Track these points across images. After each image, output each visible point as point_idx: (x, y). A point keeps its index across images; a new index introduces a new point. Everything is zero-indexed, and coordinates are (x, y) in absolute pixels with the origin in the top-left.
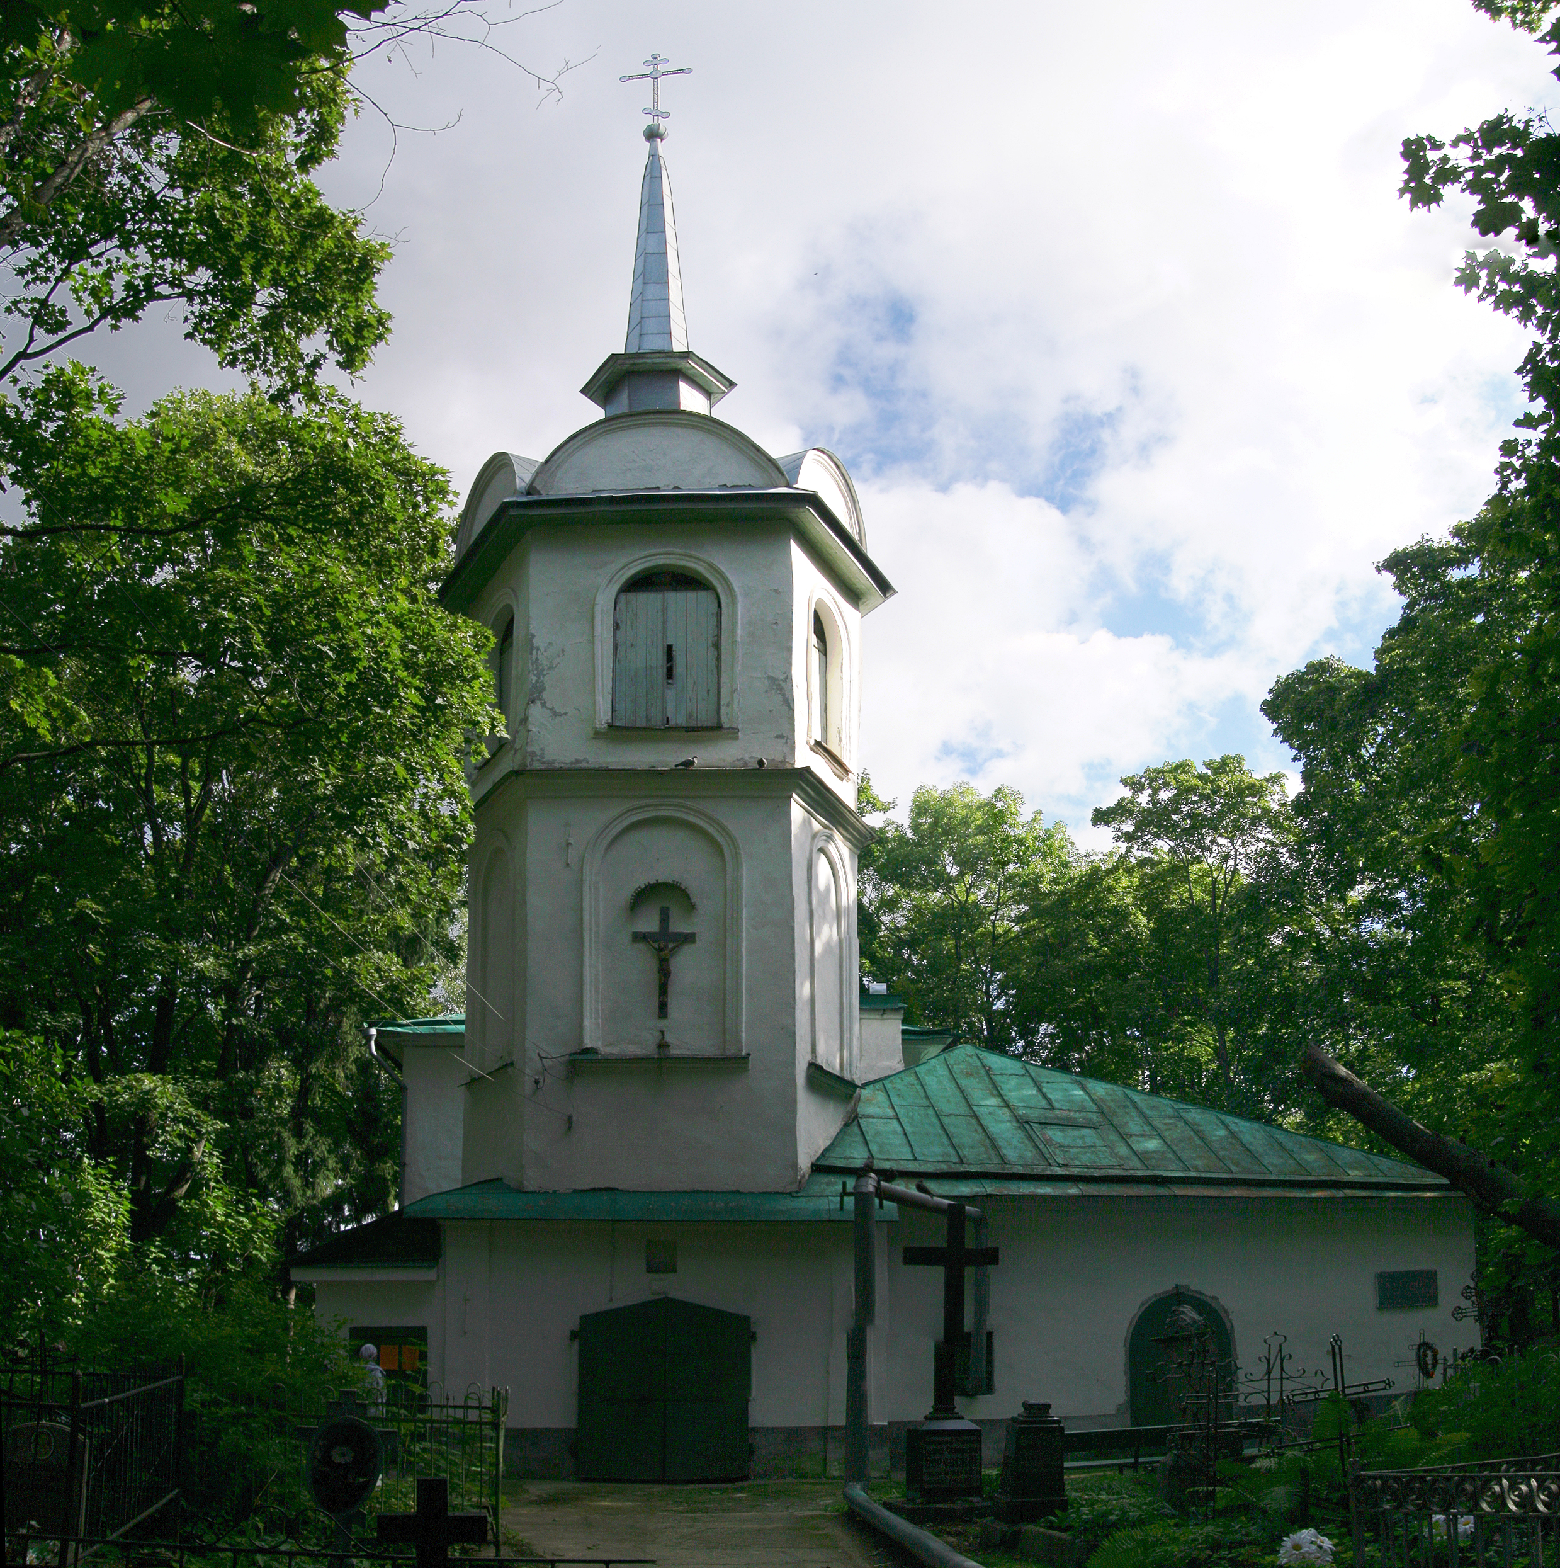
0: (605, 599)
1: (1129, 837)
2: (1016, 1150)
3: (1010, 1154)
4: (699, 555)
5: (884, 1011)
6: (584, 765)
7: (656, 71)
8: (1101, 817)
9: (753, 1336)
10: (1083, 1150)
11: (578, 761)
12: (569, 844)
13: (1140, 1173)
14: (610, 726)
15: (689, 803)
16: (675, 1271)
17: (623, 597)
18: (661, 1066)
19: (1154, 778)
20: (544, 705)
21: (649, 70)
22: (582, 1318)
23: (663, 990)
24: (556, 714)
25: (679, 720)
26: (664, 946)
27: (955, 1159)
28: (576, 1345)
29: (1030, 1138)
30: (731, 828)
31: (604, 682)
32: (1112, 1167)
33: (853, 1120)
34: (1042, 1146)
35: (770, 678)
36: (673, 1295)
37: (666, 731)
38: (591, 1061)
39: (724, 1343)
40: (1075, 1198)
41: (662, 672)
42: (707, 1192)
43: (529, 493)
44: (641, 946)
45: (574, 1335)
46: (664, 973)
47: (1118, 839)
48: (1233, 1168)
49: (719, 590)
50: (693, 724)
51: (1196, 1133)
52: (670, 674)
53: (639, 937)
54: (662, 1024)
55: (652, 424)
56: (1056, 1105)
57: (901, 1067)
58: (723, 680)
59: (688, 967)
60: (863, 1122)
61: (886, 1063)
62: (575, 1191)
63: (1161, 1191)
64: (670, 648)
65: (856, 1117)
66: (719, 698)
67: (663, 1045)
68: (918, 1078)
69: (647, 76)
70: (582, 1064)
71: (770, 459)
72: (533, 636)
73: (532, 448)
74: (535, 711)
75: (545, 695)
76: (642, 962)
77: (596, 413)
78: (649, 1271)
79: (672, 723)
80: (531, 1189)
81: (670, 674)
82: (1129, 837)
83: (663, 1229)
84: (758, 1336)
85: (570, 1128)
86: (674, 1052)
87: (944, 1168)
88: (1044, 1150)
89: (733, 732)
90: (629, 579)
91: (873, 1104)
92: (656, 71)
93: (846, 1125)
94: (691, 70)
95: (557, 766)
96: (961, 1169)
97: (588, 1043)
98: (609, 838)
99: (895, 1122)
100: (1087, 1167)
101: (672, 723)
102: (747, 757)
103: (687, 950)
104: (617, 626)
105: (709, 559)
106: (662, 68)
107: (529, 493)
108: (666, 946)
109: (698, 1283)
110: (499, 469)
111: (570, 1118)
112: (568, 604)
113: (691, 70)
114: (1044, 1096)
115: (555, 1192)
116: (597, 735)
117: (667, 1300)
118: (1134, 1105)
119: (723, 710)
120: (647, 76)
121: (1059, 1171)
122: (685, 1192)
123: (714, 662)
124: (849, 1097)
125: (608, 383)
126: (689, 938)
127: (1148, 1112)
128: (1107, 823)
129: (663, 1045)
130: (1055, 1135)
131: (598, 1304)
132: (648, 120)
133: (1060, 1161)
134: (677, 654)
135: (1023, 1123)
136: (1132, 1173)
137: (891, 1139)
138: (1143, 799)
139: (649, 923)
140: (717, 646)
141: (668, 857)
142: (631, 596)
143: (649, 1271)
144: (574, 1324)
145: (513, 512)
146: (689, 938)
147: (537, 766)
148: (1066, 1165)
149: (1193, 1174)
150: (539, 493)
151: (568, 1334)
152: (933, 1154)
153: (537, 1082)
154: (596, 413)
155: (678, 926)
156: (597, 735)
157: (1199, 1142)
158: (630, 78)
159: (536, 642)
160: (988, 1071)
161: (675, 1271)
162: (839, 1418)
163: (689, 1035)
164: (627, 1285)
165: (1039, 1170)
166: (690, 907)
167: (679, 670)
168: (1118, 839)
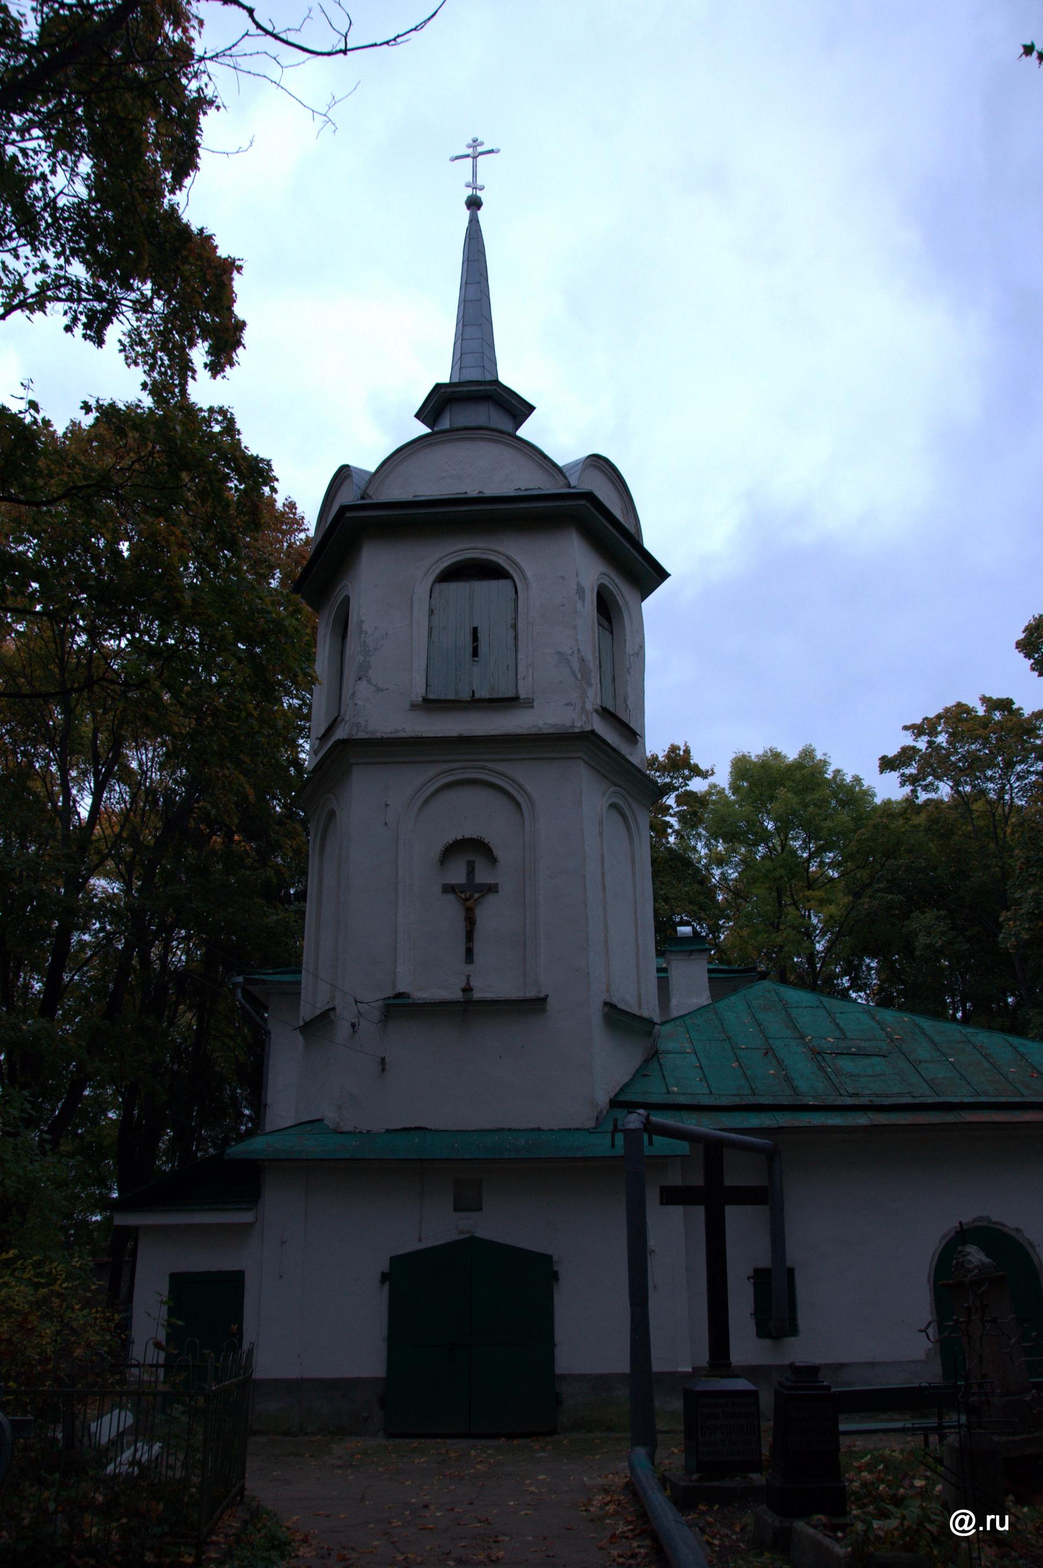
0: (422, 588)
1: (913, 780)
2: (809, 1083)
3: (803, 1086)
4: (499, 549)
5: (691, 952)
6: (402, 735)
7: (476, 152)
8: (887, 764)
9: (555, 1276)
10: (874, 1079)
11: (397, 731)
12: (387, 805)
13: (930, 1100)
14: (426, 700)
15: (490, 765)
16: (481, 1209)
17: (437, 586)
18: (466, 1009)
19: (924, 728)
20: (369, 682)
21: (470, 151)
22: (392, 1259)
23: (470, 936)
24: (379, 690)
25: (483, 693)
26: (470, 896)
27: (747, 1091)
28: (387, 1285)
29: (822, 1069)
30: (528, 787)
31: (420, 662)
32: (900, 1095)
33: (653, 1056)
34: (833, 1077)
35: (559, 653)
36: (480, 1233)
37: (476, 704)
38: (405, 1005)
39: (529, 1281)
40: (866, 1129)
41: (469, 651)
42: (510, 1130)
43: (363, 498)
44: (450, 897)
45: (384, 1277)
46: (470, 921)
47: (903, 784)
48: (1023, 1090)
49: (516, 578)
50: (495, 696)
51: (986, 1057)
52: (475, 653)
53: (449, 889)
54: (470, 967)
55: (461, 439)
56: (849, 1035)
57: (709, 1001)
58: (520, 656)
59: (492, 916)
60: (660, 1056)
61: (695, 1001)
62: (387, 1131)
63: (950, 1117)
64: (475, 630)
65: (656, 1052)
66: (516, 675)
67: (467, 990)
68: (716, 1013)
69: (468, 156)
70: (398, 1008)
71: (554, 465)
72: (362, 622)
73: (368, 459)
74: (362, 686)
75: (370, 673)
76: (451, 911)
77: (423, 430)
78: (456, 1209)
79: (477, 696)
80: (345, 1130)
81: (475, 653)
82: (913, 780)
83: (469, 1169)
84: (561, 1276)
85: (383, 1069)
86: (477, 995)
87: (737, 1101)
88: (836, 1081)
89: (529, 704)
90: (442, 571)
91: (672, 1040)
92: (476, 152)
93: (647, 1061)
94: (475, 630)
95: (379, 735)
96: (752, 1100)
97: (401, 988)
98: (422, 799)
99: (693, 1058)
100: (877, 1095)
101: (477, 696)
102: (541, 723)
103: (491, 898)
104: (432, 612)
105: (508, 553)
106: (480, 149)
107: (363, 498)
108: (471, 897)
109: (507, 1223)
110: (345, 478)
111: (383, 1059)
112: (388, 590)
113: (498, 151)
114: (837, 1025)
115: (368, 1132)
116: (414, 707)
117: (473, 1239)
118: (923, 1032)
119: (521, 683)
120: (468, 156)
121: (849, 1101)
122: (490, 1131)
123: (513, 641)
124: (649, 1034)
125: (437, 405)
126: (492, 889)
127: (936, 1039)
128: (893, 769)
129: (467, 990)
130: (846, 1064)
131: (409, 1245)
132: (469, 192)
133: (850, 1090)
134: (482, 636)
135: (816, 1053)
136: (922, 1100)
137: (686, 1074)
138: (922, 744)
139: (457, 875)
140: (515, 627)
141: (474, 815)
142: (444, 586)
143: (456, 1209)
144: (384, 1266)
145: (348, 515)
146: (492, 889)
147: (361, 735)
148: (857, 1095)
149: (982, 1099)
150: (370, 497)
151: (378, 1277)
152: (728, 1088)
153: (353, 1026)
154: (423, 430)
155: (482, 877)
156: (414, 707)
157: (987, 1065)
158: (457, 158)
159: (365, 627)
160: (786, 1006)
161: (481, 1209)
162: (623, 1366)
163: (494, 983)
164: (430, 1224)
165: (829, 1101)
166: (493, 860)
167: (483, 649)
168: (903, 784)
